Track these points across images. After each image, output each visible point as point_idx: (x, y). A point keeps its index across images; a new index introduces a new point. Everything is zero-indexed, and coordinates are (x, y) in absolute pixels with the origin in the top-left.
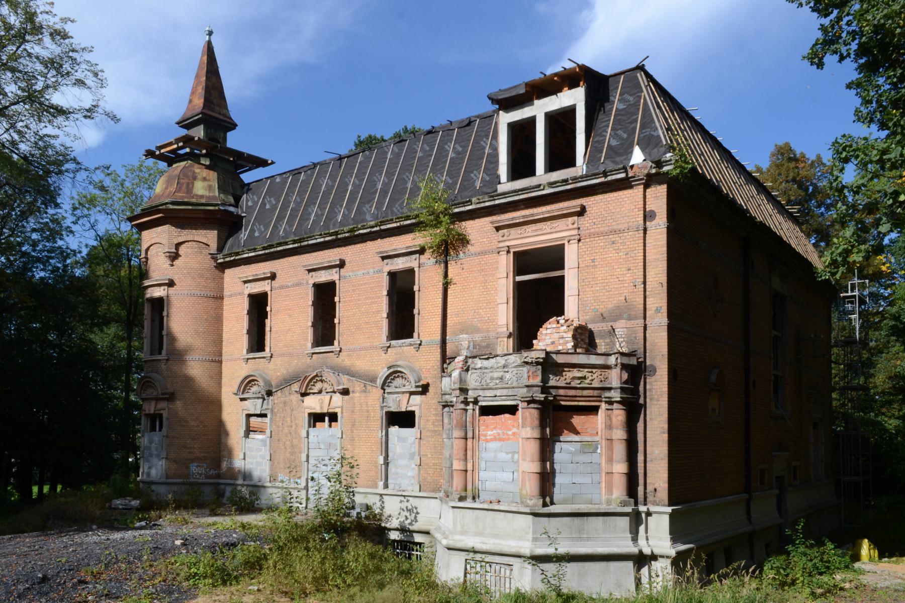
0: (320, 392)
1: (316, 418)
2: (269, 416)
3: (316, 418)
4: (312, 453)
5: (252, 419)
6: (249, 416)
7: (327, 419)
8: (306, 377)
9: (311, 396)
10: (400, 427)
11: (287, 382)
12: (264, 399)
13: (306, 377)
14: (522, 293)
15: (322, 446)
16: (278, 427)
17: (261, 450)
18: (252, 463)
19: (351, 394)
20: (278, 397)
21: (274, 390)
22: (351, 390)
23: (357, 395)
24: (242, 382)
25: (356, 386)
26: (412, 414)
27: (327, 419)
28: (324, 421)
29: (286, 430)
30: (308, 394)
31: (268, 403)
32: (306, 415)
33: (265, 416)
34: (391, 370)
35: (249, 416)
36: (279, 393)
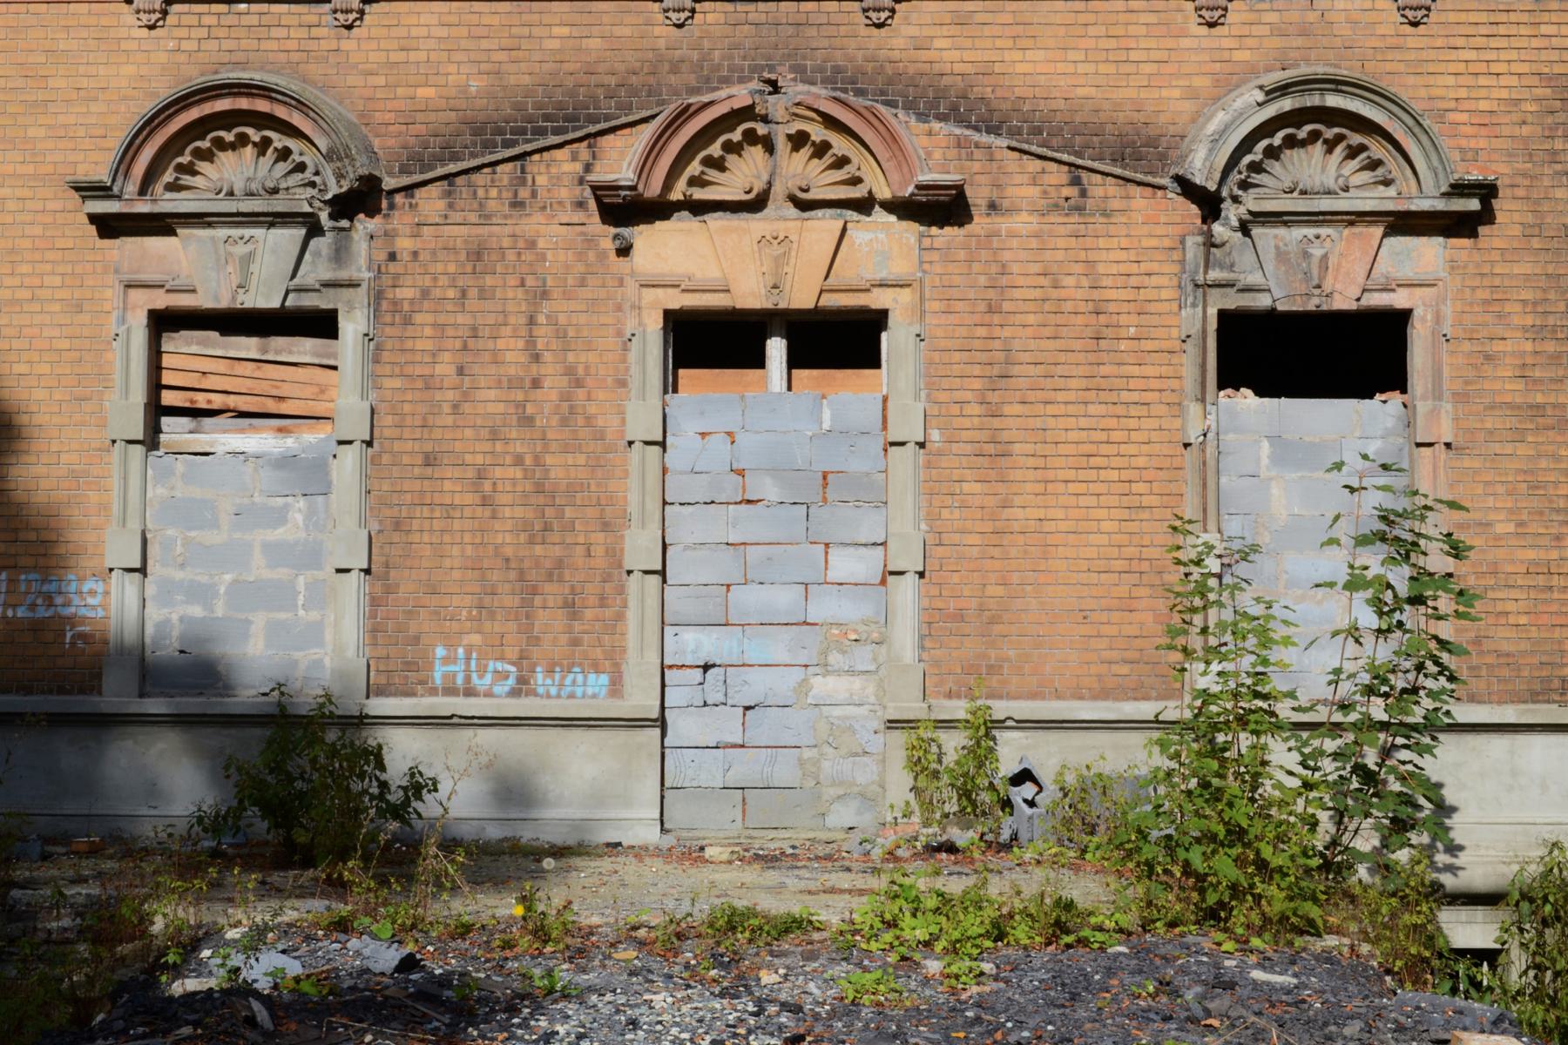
0: (756, 204)
1: (710, 340)
2: (352, 327)
3: (710, 340)
4: (687, 527)
5: (183, 349)
6: (164, 322)
7: (776, 349)
8: (684, 114)
9: (682, 223)
10: (1261, 392)
11: (501, 139)
12: (315, 229)
13: (684, 114)
14: (1448, 643)
15: (770, 490)
16: (429, 384)
17: (280, 517)
18: (200, 593)
19: (980, 223)
20: (422, 224)
21: (389, 183)
22: (977, 196)
23: (1023, 222)
24: (151, 124)
25: (1019, 190)
26: (1231, 376)
27: (776, 349)
28: (757, 360)
29: (491, 402)
30: (658, 210)
31: (340, 255)
32: (655, 324)
33: (323, 325)
34: (1286, 104)
35: (164, 322)
36: (431, 201)
